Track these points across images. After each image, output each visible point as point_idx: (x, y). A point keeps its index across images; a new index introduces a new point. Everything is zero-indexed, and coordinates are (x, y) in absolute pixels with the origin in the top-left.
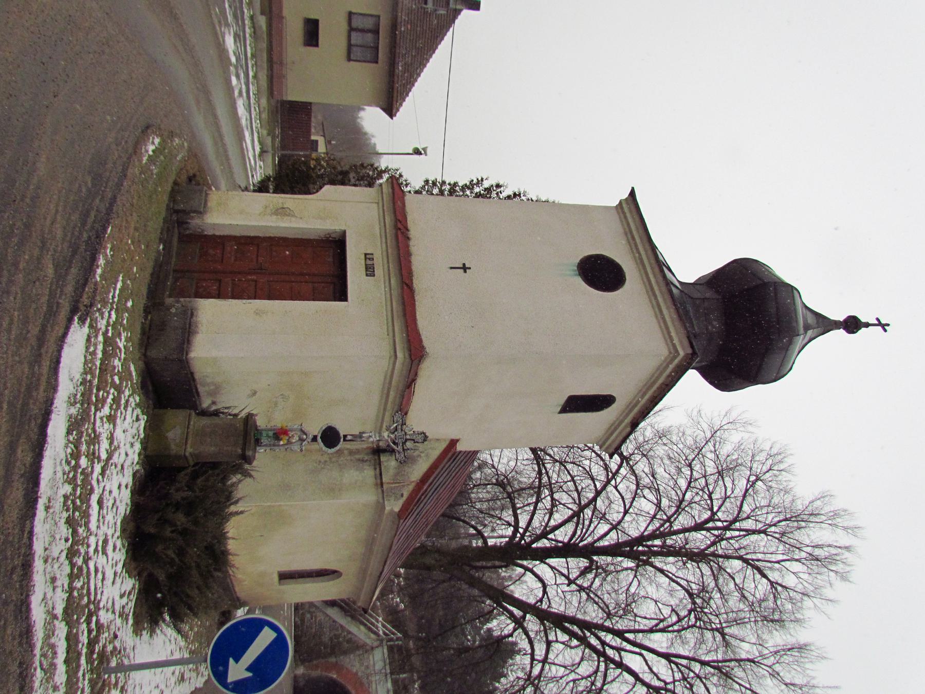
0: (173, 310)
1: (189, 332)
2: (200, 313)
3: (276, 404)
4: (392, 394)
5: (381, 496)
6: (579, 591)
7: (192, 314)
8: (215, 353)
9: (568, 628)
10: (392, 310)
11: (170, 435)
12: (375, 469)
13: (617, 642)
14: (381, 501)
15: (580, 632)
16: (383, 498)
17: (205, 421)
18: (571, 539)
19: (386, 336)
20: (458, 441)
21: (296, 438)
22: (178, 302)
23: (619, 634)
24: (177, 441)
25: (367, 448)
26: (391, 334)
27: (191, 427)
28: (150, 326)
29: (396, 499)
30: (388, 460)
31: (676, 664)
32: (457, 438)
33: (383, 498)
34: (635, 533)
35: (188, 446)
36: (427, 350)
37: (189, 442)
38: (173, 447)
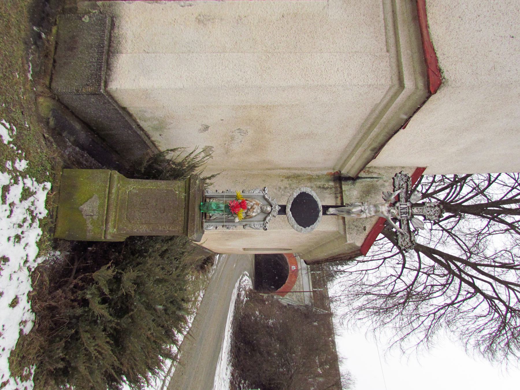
0: (86, 19)
1: (109, 51)
2: (123, 22)
3: (233, 138)
4: (376, 130)
5: (342, 227)
6: (442, 230)
7: (113, 25)
8: (144, 83)
9: (434, 257)
10: (394, 12)
11: (86, 208)
12: (337, 197)
13: (473, 272)
14: (342, 232)
15: (444, 262)
16: (345, 230)
17: (134, 186)
18: (445, 199)
19: (384, 53)
20: (424, 169)
21: (257, 209)
22: (95, 7)
23: (474, 266)
24: (95, 217)
25: (328, 175)
26: (393, 50)
27: (113, 196)
28: (57, 43)
29: (358, 232)
30: (350, 190)
31: (513, 290)
32: (425, 166)
33: (345, 230)
34: (496, 198)
35: (110, 224)
36: (446, 75)
37: (112, 218)
38: (90, 226)
